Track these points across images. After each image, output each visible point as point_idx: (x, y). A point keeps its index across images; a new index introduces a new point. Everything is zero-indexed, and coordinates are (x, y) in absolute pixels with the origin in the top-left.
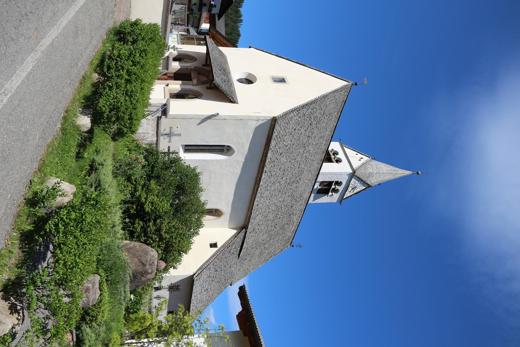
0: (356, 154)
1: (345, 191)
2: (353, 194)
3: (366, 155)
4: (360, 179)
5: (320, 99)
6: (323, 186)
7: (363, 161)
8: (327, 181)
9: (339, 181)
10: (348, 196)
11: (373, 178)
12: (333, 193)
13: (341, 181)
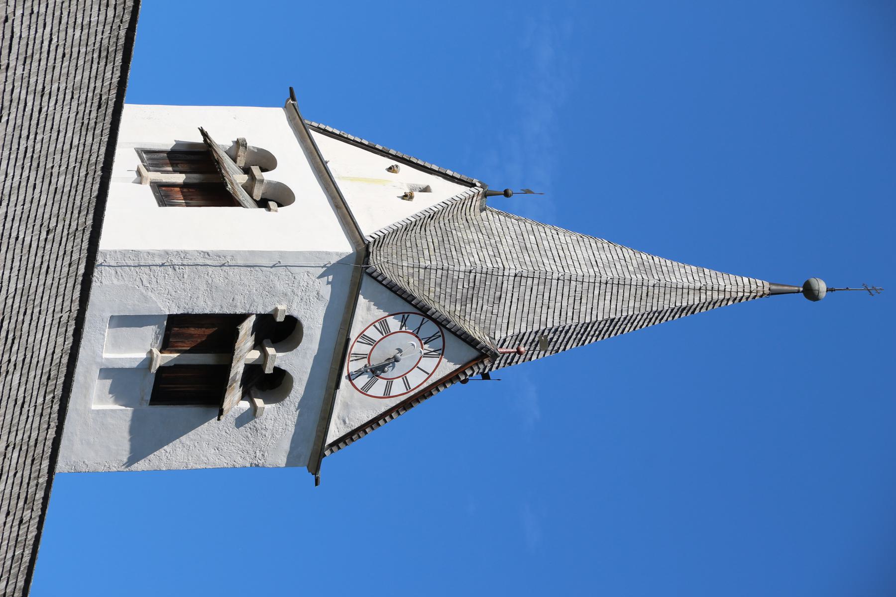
0: (391, 169)
1: (328, 389)
2: (388, 413)
3: (449, 172)
4: (408, 298)
5: (422, 221)
6: (192, 351)
7: (422, 204)
8: (207, 311)
9: (276, 310)
10: (356, 425)
11: (503, 308)
12: (259, 402)
13: (295, 314)
